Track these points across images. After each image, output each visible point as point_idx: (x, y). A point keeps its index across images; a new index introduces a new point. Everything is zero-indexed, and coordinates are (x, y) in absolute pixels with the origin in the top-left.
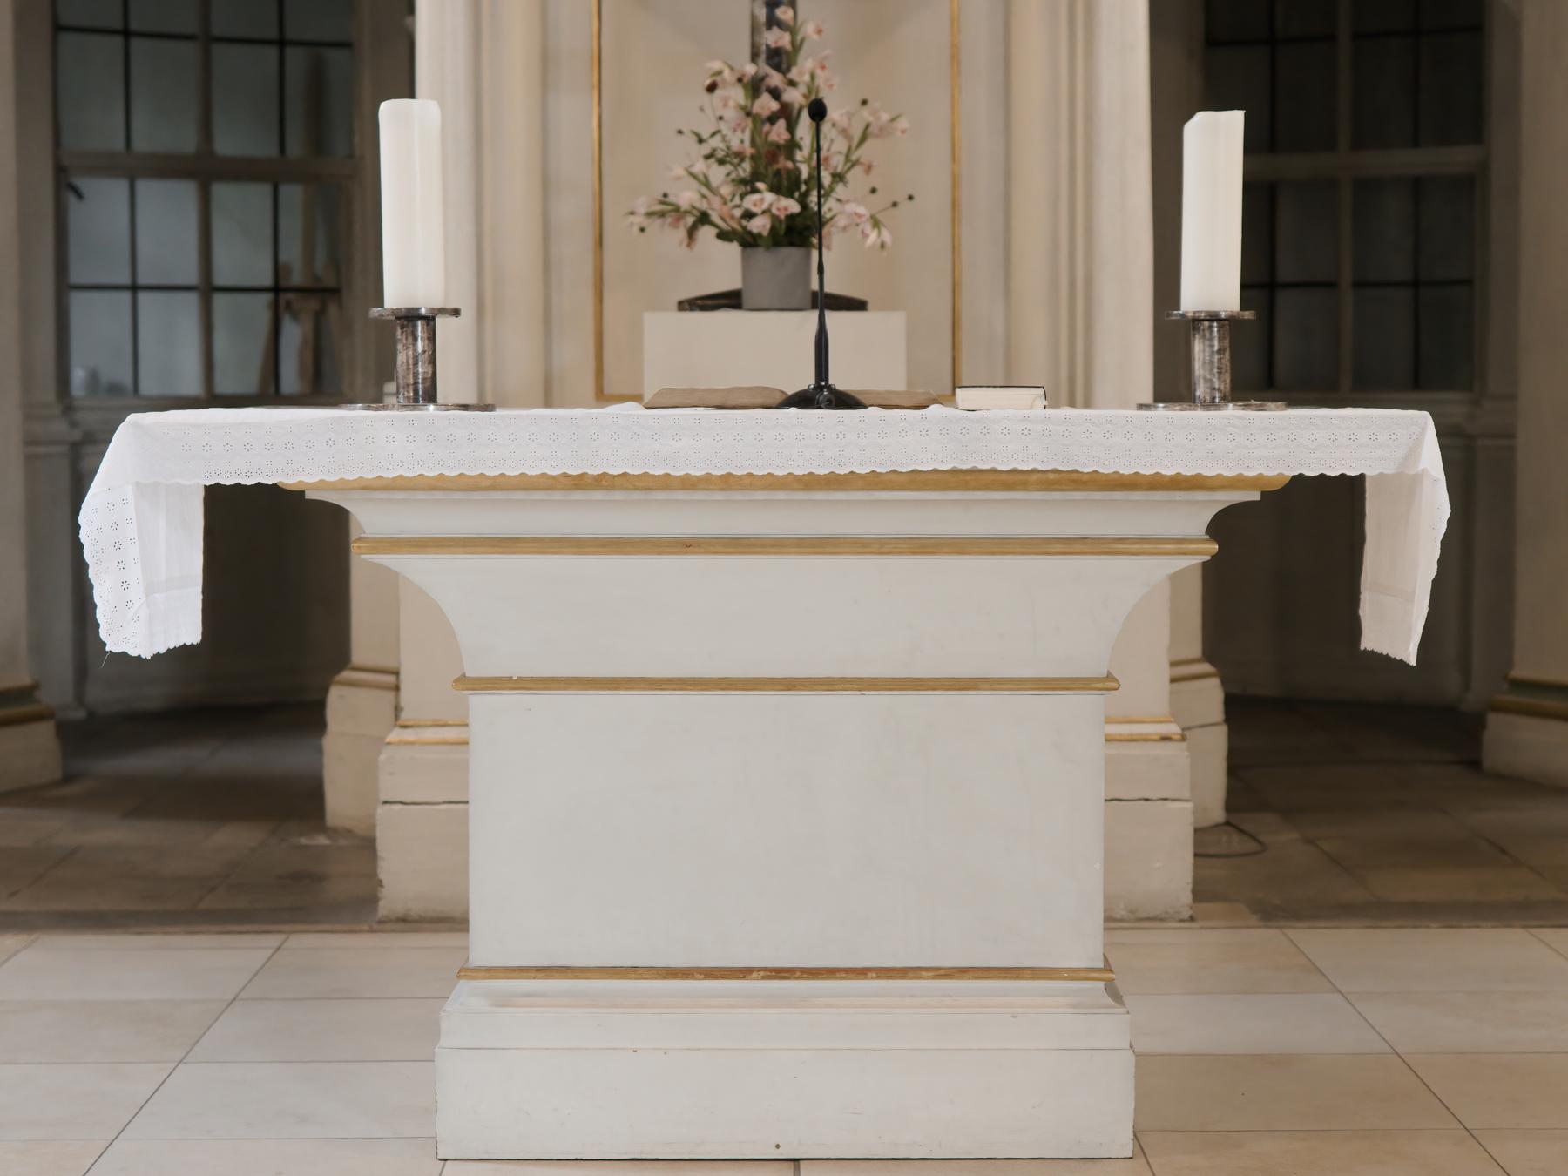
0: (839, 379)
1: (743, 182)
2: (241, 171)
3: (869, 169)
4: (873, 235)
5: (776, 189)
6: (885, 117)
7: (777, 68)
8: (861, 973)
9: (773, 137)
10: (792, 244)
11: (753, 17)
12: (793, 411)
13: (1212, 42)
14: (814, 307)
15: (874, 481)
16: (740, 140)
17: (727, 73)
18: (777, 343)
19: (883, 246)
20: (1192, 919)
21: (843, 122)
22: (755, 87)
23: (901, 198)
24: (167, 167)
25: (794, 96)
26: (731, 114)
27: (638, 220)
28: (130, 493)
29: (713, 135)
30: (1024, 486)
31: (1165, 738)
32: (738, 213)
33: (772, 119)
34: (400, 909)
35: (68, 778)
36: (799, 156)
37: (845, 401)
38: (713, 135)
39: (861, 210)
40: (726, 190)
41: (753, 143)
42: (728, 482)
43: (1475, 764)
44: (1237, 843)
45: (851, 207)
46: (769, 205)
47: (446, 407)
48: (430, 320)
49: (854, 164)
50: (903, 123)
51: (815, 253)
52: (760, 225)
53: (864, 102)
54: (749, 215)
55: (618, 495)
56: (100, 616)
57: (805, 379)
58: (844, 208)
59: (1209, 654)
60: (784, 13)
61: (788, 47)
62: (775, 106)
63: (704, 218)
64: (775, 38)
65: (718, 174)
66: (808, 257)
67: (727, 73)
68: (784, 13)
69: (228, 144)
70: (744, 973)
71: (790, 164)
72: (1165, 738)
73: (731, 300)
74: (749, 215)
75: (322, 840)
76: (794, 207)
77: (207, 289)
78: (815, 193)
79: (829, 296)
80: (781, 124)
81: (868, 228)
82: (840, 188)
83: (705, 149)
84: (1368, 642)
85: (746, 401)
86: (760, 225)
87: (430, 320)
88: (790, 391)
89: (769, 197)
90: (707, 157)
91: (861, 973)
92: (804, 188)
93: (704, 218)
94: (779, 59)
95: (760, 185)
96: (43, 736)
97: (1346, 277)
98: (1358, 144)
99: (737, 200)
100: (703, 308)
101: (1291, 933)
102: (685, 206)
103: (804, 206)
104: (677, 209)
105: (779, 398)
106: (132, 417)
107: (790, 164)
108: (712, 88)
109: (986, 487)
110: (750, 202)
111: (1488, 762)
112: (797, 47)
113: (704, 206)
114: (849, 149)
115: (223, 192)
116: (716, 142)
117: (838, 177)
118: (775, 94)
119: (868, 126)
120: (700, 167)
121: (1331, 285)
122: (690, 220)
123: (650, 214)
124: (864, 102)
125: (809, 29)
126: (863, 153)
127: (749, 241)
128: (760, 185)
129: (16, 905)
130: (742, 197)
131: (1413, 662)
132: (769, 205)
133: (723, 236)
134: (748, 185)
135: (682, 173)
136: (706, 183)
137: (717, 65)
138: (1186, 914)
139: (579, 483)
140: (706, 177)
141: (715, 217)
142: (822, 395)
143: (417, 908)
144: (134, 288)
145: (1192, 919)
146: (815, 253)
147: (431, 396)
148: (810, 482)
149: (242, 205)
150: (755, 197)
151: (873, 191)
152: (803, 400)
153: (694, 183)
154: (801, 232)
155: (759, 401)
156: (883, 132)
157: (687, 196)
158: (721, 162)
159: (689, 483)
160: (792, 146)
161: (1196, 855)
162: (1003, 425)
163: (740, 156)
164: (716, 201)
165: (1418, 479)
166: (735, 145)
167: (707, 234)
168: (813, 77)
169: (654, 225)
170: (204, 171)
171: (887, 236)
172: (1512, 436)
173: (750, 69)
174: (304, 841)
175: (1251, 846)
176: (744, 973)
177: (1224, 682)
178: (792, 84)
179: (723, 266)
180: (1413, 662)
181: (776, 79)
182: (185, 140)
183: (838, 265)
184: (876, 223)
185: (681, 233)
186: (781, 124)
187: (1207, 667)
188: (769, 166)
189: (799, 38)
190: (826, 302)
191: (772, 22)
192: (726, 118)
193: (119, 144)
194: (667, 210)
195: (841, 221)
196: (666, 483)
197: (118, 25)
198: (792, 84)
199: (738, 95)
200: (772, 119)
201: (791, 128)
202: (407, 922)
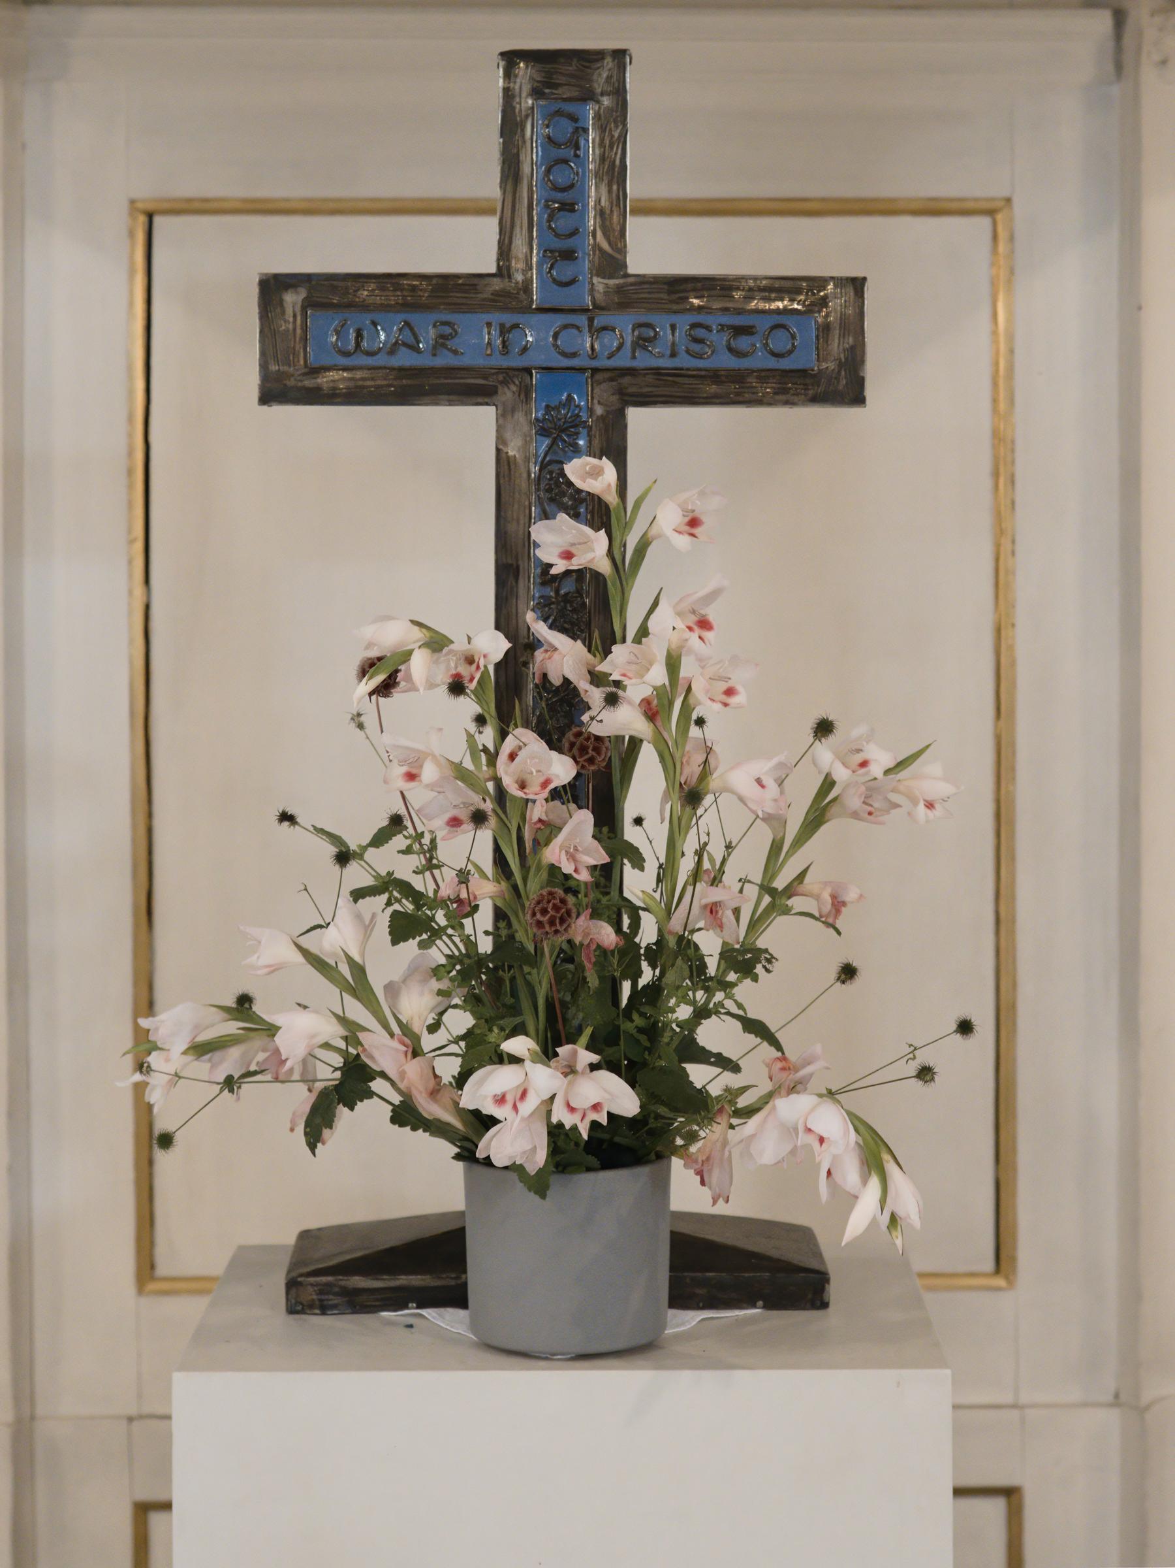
3: (831, 916)
6: (881, 759)
12: (921, 747)
29: (380, 839)
38: (380, 839)
40: (416, 1005)
46: (543, 1091)
53: (824, 728)
60: (590, 474)
61: (604, 567)
64: (559, 541)
65: (389, 962)
67: (419, 665)
83: (357, 875)
89: (543, 1079)
92: (647, 975)
94: (588, 607)
95: (518, 1045)
112: (625, 567)
114: (776, 848)
119: (828, 784)
120: (340, 939)
124: (824, 728)
133: (405, 1115)
135: (283, 934)
136: (357, 983)
140: (359, 970)
151: (848, 972)
153: (328, 994)
161: (168, 1417)
168: (673, 665)
181: (563, 656)
189: (632, 541)
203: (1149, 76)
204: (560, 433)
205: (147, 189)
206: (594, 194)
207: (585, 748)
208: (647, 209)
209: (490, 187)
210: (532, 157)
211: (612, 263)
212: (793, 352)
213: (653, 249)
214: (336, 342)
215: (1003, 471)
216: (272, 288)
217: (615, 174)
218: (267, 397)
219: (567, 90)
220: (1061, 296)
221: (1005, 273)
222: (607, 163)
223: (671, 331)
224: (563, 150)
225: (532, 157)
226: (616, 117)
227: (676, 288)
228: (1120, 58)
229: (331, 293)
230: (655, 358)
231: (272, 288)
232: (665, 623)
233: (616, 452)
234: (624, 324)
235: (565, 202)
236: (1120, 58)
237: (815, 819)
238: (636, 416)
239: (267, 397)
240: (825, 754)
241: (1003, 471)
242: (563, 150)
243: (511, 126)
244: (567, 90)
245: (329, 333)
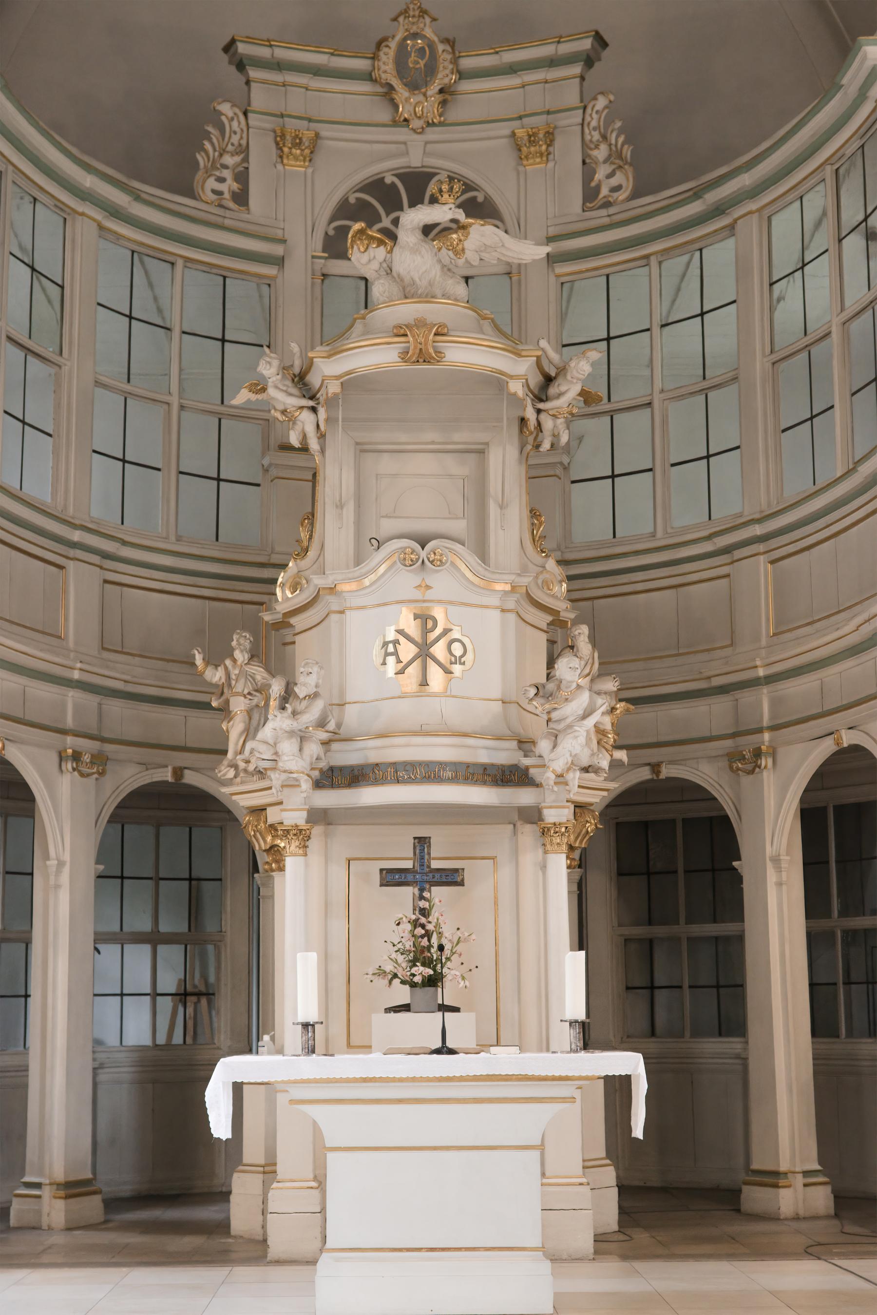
0: (450, 1044)
1: (410, 961)
2: (170, 939)
4: (462, 983)
5: (423, 965)
6: (467, 934)
7: (424, 915)
8: (459, 1249)
9: (422, 944)
10: (430, 986)
11: (414, 894)
13: (620, 874)
14: (439, 1010)
15: (461, 1079)
16: (409, 945)
17: (404, 919)
18: (424, 1026)
19: (610, 101)
20: (594, 1259)
21: (450, 937)
22: (415, 924)
23: (473, 967)
24: (139, 938)
25: (430, 927)
26: (407, 935)
27: (370, 977)
28: (221, 1085)
30: (511, 1080)
31: (581, 1184)
32: (409, 974)
33: (422, 937)
34: (276, 1258)
35: (106, 1221)
36: (433, 950)
37: (452, 1052)
39: (458, 973)
40: (404, 965)
41: (414, 945)
42: (414, 1079)
43: (738, 1211)
44: (622, 1237)
45: (453, 972)
46: (421, 971)
47: (319, 1055)
48: (313, 1025)
49: (454, 953)
50: (473, 937)
51: (440, 990)
52: (418, 979)
53: (458, 929)
54: (414, 975)
55: (377, 1084)
56: (211, 1125)
57: (439, 1044)
58: (451, 972)
59: (609, 1156)
60: (426, 894)
62: (423, 932)
63: (395, 976)
64: (423, 904)
65: (400, 958)
66: (437, 990)
67: (404, 919)
68: (426, 894)
69: (164, 928)
70: (419, 1250)
71: (429, 955)
72: (581, 1184)
73: (406, 1008)
74: (414, 975)
75: (230, 1240)
76: (431, 972)
77: (155, 995)
78: (439, 965)
79: (447, 1006)
80: (426, 938)
81: (460, 980)
82: (449, 963)
83: (396, 948)
84: (633, 1135)
85: (417, 1052)
86: (418, 979)
87: (313, 1025)
88: (433, 1048)
89: (421, 968)
90: (396, 951)
91: (459, 1249)
92: (278, 139)
93: (395, 976)
94: (424, 912)
95: (418, 964)
96: (96, 1201)
97: (686, 985)
98: (689, 921)
99: (408, 969)
100: (395, 1012)
101: (633, 1264)
102: (388, 971)
103: (435, 970)
104: (385, 972)
105: (429, 1051)
106: (222, 1060)
107: (429, 955)
108: (398, 924)
109: (498, 1080)
110: (414, 970)
111: (742, 1209)
112: (431, 907)
113: (396, 971)
115: (161, 949)
116: (400, 946)
117: (448, 959)
118: (423, 926)
120: (394, 956)
121: (680, 987)
122: (390, 977)
123: (374, 974)
124: (458, 929)
125: (436, 901)
126: (459, 949)
127: (413, 985)
128: (418, 964)
129: (114, 1260)
130: (411, 968)
131: (641, 1138)
132: (421, 971)
133: (403, 982)
134: (413, 963)
136: (396, 962)
137: (401, 916)
138: (592, 1257)
139: (365, 1080)
141: (400, 976)
142: (444, 1050)
143: (283, 1256)
144: (122, 995)
145: (594, 1259)
146: (440, 990)
147: (313, 1052)
148: (441, 1079)
149: (171, 954)
150: (416, 968)
152: (438, 1052)
154: (434, 981)
155: (422, 1051)
156: (466, 940)
157: (389, 967)
158: (402, 954)
159: (401, 1080)
160: (430, 946)
162: (505, 1059)
163: (410, 951)
164: (400, 969)
165: (639, 1075)
166: (408, 947)
167: (396, 981)
169: (376, 979)
170: (154, 939)
171: (467, 983)
172: (27, 1070)
173: (414, 917)
174: (223, 1241)
175: (628, 1238)
176: (419, 1250)
177: (617, 1169)
178: (430, 922)
179: (402, 994)
180: (641, 1138)
181: (423, 920)
182: (145, 925)
183: (448, 994)
184: (463, 978)
185: (386, 982)
186: (426, 938)
187: (608, 1162)
188: (420, 956)
190: (444, 1008)
191: (422, 898)
192: (403, 935)
193: (117, 928)
194: (381, 972)
195: (449, 977)
196: (394, 1080)
197: (120, 875)
198: (430, 922)
199: (409, 927)
200: (422, 937)
201: (429, 941)
202: (278, 1262)
203: (520, 835)
204: (422, 890)
205: (349, 856)
206: (426, 857)
207: (427, 931)
208: (434, 859)
209: (411, 855)
210: (418, 851)
211: (429, 867)
212: (451, 878)
213: (435, 865)
214: (392, 878)
215: (496, 903)
216: (381, 870)
217: (429, 854)
218: (382, 885)
219: (422, 842)
220: (505, 872)
221: (495, 870)
222: (254, 693)
223: (437, 876)
224: (422, 851)
225: (418, 851)
226: (429, 846)
227: (438, 870)
228: (515, 832)
229: (390, 871)
230: (435, 880)
231: (381, 870)
232: (436, 915)
233: (430, 891)
234: (431, 875)
235: (422, 858)
236: (515, 832)
237: (457, 944)
238: (432, 888)
239: (382, 885)
240: (458, 932)
241: (496, 903)
242: (422, 851)
243: (415, 848)
244: (422, 842)
245: (389, 877)
